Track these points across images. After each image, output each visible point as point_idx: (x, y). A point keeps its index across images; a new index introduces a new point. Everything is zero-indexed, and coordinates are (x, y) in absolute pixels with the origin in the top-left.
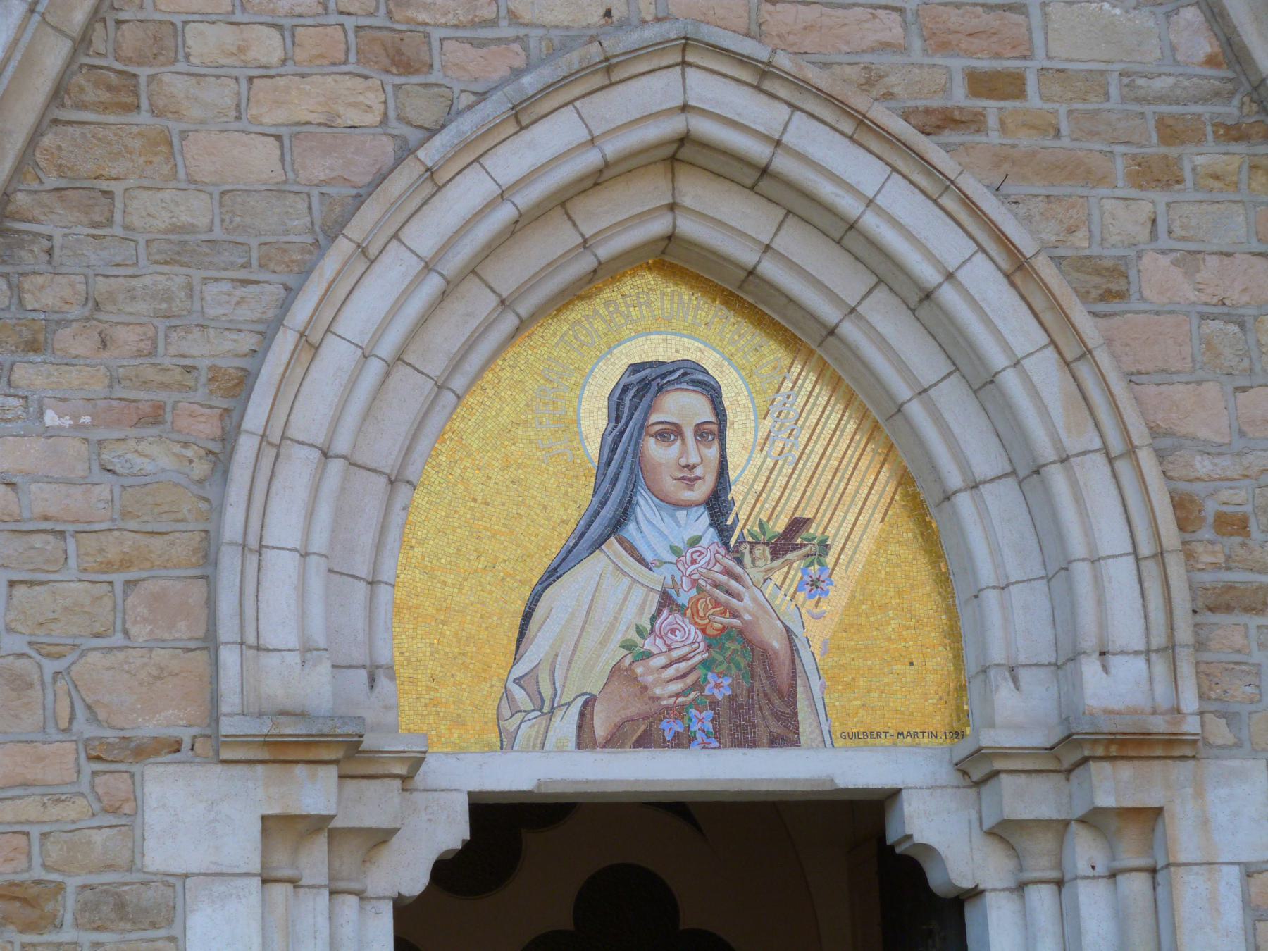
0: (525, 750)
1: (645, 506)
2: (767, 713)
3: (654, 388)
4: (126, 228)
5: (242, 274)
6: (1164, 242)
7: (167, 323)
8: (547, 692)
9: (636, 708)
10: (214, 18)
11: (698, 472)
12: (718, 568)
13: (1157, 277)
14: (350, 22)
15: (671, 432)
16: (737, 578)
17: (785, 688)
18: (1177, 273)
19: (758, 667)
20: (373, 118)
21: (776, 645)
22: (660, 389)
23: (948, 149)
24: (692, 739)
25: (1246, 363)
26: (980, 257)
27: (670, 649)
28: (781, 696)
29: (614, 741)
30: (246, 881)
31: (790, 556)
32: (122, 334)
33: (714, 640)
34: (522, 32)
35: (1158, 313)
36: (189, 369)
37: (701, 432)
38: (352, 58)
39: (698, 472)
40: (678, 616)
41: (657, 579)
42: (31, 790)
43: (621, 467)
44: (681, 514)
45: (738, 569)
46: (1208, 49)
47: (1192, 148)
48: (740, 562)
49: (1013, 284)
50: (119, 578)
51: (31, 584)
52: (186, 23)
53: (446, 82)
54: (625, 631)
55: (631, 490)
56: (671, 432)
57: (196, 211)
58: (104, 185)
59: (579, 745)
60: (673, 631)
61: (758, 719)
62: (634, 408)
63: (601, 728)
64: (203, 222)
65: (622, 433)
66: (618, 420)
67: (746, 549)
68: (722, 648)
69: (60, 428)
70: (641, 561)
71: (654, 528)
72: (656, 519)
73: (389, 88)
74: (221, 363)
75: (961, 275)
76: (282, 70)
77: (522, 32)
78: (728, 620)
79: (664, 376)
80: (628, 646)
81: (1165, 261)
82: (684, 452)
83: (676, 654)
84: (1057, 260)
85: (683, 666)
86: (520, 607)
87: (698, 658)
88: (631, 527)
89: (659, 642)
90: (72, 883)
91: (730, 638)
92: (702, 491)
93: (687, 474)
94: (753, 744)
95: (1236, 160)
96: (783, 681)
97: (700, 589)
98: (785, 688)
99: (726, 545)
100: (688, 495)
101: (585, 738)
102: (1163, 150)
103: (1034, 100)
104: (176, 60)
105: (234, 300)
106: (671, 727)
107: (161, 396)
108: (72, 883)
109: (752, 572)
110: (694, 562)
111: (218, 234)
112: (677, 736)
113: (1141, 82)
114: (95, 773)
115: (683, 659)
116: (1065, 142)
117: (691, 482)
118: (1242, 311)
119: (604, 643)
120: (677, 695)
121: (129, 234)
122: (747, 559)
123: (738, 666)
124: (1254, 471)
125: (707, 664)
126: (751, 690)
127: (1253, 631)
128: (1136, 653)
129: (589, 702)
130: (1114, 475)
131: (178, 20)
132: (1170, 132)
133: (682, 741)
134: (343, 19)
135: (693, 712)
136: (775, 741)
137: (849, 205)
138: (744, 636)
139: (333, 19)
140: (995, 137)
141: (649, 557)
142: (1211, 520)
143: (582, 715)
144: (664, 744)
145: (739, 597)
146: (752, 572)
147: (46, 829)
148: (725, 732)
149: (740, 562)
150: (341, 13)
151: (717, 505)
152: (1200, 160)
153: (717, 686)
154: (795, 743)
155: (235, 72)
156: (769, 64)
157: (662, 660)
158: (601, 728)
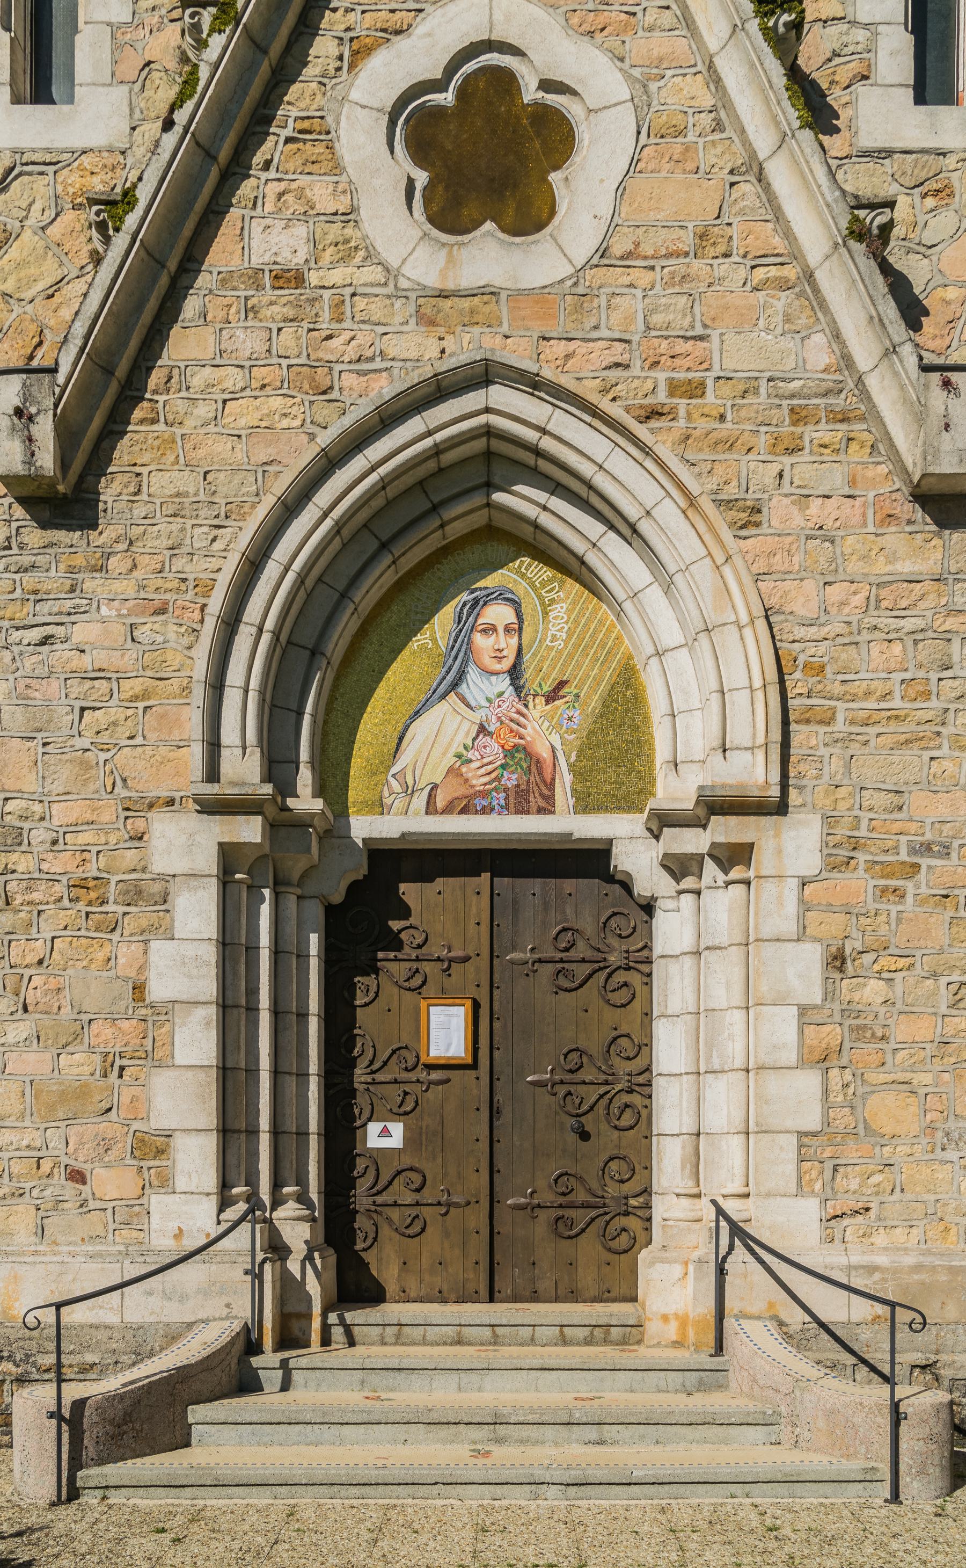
0: (396, 815)
1: (473, 674)
2: (537, 795)
3: (481, 603)
4: (149, 495)
5: (216, 522)
6: (787, 488)
7: (172, 552)
8: (410, 783)
9: (462, 791)
10: (203, 363)
11: (505, 653)
12: (514, 710)
13: (780, 512)
14: (285, 362)
15: (490, 629)
16: (523, 715)
17: (549, 781)
18: (795, 510)
19: (533, 769)
20: (297, 423)
21: (545, 755)
22: (485, 604)
23: (652, 431)
24: (492, 809)
25: (833, 566)
26: (668, 500)
27: (483, 757)
28: (546, 785)
29: (448, 810)
30: (208, 879)
31: (556, 703)
32: (143, 560)
33: (510, 752)
34: (389, 364)
35: (779, 535)
36: (184, 580)
37: (507, 629)
38: (286, 385)
39: (505, 653)
40: (488, 738)
41: (477, 717)
42: (92, 827)
43: (459, 650)
44: (494, 678)
45: (525, 710)
46: (828, 361)
47: (810, 427)
48: (526, 706)
49: (687, 517)
50: (141, 705)
51: (94, 709)
52: (187, 366)
53: (342, 398)
54: (457, 747)
55: (465, 663)
56: (490, 629)
57: (189, 482)
58: (137, 469)
59: (427, 813)
60: (485, 747)
61: (532, 799)
62: (469, 616)
63: (440, 803)
64: (191, 490)
65: (461, 631)
66: (459, 622)
67: (530, 698)
68: (513, 757)
69: (110, 616)
70: (468, 706)
71: (478, 687)
72: (478, 682)
73: (307, 404)
74: (201, 576)
75: (653, 513)
76: (243, 394)
77: (389, 364)
78: (517, 741)
79: (488, 595)
80: (459, 756)
81: (786, 501)
82: (497, 642)
83: (486, 761)
84: (718, 503)
85: (490, 768)
86: (396, 735)
87: (499, 763)
88: (464, 685)
89: (477, 753)
90: (114, 879)
91: (518, 751)
92: (507, 664)
93: (498, 654)
94: (528, 812)
95: (840, 434)
96: (548, 777)
97: (502, 722)
98: (549, 781)
99: (519, 696)
100: (497, 667)
101: (431, 809)
102: (792, 429)
103: (710, 397)
104: (180, 390)
105: (210, 537)
106: (480, 803)
107: (168, 596)
108: (114, 879)
109: (534, 712)
110: (499, 706)
111: (202, 497)
112: (484, 807)
113: (781, 384)
114: (126, 818)
115: (490, 763)
116: (729, 425)
117: (500, 659)
118: (834, 533)
119: (444, 754)
120: (485, 784)
121: (151, 499)
122: (531, 705)
123: (521, 767)
124: (832, 635)
125: (503, 766)
126: (528, 782)
127: (821, 736)
128: (746, 749)
129: (435, 787)
130: (742, 638)
131: (182, 365)
132: (798, 416)
133: (485, 811)
134: (282, 361)
135: (494, 794)
136: (541, 811)
137: (632, 511)
138: (526, 751)
139: (275, 360)
140: (682, 423)
141: (473, 703)
142: (801, 666)
143: (430, 795)
144: (476, 812)
145: (525, 727)
146: (534, 712)
147: (100, 848)
148: (512, 806)
149: (526, 706)
150: (280, 357)
151: (515, 672)
152: (815, 435)
153: (509, 779)
154: (553, 812)
155: (214, 397)
156: (538, 375)
157: (478, 764)
158: (440, 803)
